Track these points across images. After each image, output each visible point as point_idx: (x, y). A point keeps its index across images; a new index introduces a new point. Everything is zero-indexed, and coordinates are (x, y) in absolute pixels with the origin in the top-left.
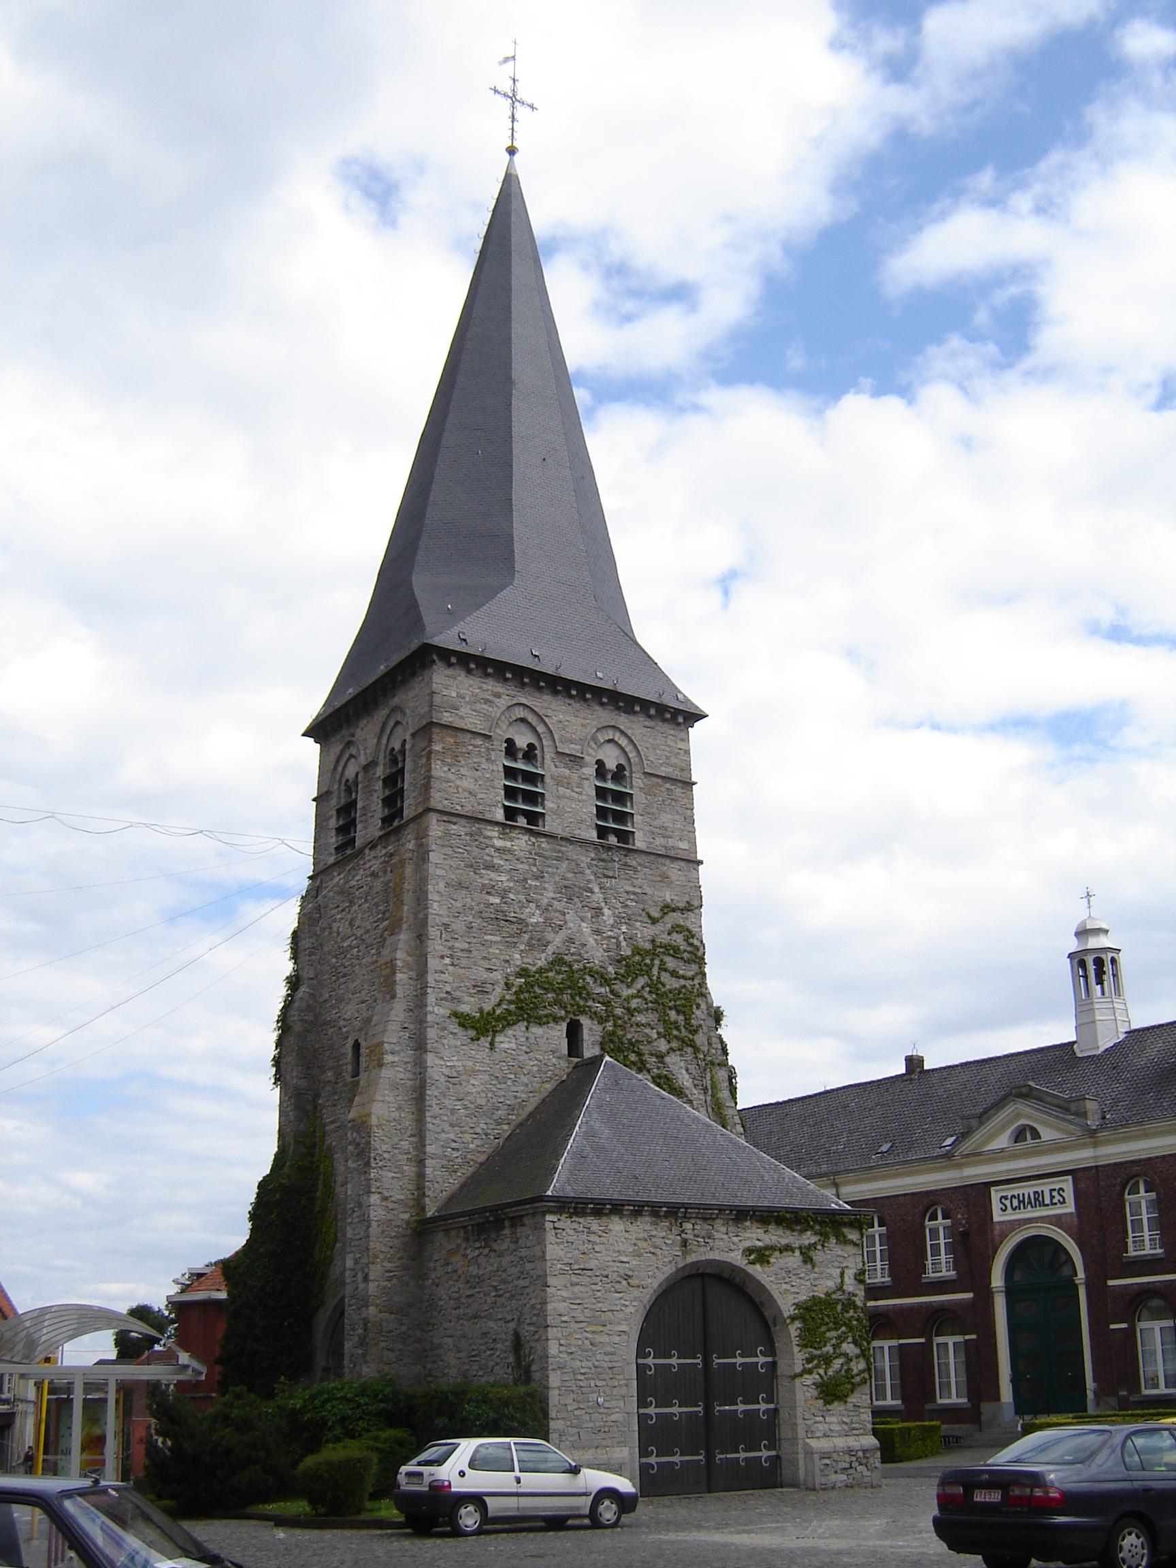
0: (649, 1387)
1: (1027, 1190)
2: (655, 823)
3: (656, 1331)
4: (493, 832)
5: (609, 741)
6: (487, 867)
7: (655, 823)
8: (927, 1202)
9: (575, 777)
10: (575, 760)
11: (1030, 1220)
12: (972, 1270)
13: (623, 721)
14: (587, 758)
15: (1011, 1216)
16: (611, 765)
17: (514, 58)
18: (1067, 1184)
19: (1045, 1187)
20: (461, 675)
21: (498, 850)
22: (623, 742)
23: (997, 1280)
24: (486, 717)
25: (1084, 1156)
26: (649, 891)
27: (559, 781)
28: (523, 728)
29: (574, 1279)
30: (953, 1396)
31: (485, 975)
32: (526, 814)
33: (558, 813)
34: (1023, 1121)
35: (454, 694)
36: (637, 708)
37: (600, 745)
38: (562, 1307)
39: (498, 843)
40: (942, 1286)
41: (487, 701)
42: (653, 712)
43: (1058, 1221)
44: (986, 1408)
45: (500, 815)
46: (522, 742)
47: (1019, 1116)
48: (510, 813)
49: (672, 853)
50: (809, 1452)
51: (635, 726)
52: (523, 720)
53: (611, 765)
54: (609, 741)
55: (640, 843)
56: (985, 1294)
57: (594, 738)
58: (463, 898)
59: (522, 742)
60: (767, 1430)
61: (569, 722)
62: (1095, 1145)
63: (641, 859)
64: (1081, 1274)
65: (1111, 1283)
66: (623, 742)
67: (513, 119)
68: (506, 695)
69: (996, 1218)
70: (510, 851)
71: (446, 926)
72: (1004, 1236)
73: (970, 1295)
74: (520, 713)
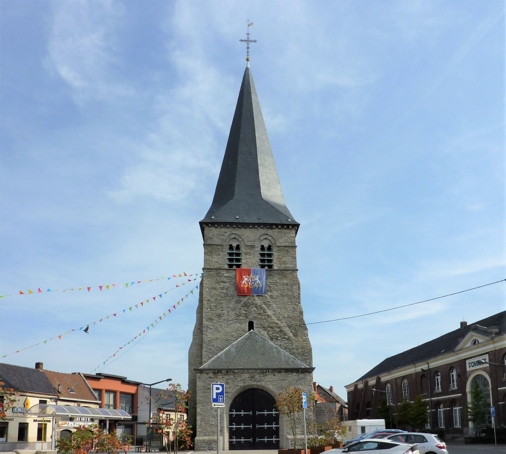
0: (232, 420)
1: (475, 360)
2: (282, 260)
3: (235, 405)
4: (224, 272)
5: (266, 239)
6: (222, 282)
7: (282, 260)
8: (450, 367)
9: (252, 251)
10: (252, 247)
11: (477, 370)
12: (462, 388)
13: (270, 232)
14: (256, 245)
15: (472, 368)
16: (266, 246)
17: (249, 26)
18: (487, 357)
19: (480, 359)
20: (213, 229)
21: (225, 277)
22: (270, 238)
23: (468, 389)
24: (222, 240)
25: (490, 347)
26: (278, 281)
27: (246, 254)
28: (235, 240)
29: (205, 391)
30: (458, 426)
31: (221, 312)
32: (236, 265)
33: (246, 263)
34: (474, 338)
35: (211, 235)
36: (274, 227)
37: (261, 241)
38: (202, 399)
39: (225, 275)
40: (454, 392)
41: (222, 235)
42: (280, 227)
43: (484, 369)
44: (465, 429)
45: (226, 267)
46: (234, 245)
47: (473, 336)
48: (231, 266)
49: (288, 269)
50: (288, 439)
51: (274, 233)
52: (235, 238)
53: (266, 246)
54: (266, 239)
55: (275, 267)
56: (465, 394)
57: (259, 239)
58: (213, 292)
59: (234, 245)
60: (276, 433)
61: (248, 236)
62: (494, 343)
63: (276, 272)
64: (491, 386)
65: (499, 389)
66: (270, 238)
67: (248, 48)
68: (228, 231)
69: (468, 370)
70: (229, 277)
71: (209, 300)
72: (470, 375)
73: (461, 394)
74: (233, 236)
